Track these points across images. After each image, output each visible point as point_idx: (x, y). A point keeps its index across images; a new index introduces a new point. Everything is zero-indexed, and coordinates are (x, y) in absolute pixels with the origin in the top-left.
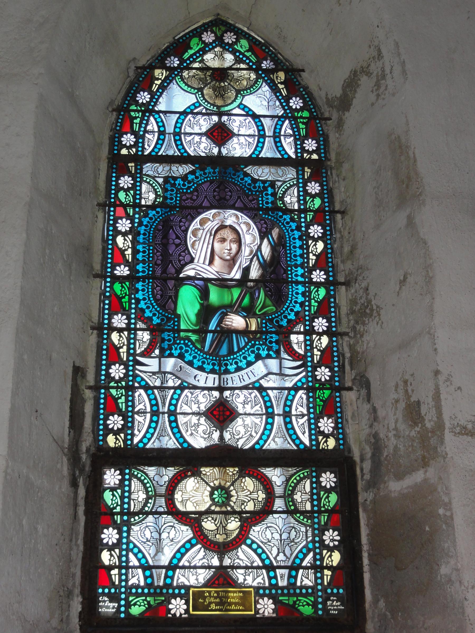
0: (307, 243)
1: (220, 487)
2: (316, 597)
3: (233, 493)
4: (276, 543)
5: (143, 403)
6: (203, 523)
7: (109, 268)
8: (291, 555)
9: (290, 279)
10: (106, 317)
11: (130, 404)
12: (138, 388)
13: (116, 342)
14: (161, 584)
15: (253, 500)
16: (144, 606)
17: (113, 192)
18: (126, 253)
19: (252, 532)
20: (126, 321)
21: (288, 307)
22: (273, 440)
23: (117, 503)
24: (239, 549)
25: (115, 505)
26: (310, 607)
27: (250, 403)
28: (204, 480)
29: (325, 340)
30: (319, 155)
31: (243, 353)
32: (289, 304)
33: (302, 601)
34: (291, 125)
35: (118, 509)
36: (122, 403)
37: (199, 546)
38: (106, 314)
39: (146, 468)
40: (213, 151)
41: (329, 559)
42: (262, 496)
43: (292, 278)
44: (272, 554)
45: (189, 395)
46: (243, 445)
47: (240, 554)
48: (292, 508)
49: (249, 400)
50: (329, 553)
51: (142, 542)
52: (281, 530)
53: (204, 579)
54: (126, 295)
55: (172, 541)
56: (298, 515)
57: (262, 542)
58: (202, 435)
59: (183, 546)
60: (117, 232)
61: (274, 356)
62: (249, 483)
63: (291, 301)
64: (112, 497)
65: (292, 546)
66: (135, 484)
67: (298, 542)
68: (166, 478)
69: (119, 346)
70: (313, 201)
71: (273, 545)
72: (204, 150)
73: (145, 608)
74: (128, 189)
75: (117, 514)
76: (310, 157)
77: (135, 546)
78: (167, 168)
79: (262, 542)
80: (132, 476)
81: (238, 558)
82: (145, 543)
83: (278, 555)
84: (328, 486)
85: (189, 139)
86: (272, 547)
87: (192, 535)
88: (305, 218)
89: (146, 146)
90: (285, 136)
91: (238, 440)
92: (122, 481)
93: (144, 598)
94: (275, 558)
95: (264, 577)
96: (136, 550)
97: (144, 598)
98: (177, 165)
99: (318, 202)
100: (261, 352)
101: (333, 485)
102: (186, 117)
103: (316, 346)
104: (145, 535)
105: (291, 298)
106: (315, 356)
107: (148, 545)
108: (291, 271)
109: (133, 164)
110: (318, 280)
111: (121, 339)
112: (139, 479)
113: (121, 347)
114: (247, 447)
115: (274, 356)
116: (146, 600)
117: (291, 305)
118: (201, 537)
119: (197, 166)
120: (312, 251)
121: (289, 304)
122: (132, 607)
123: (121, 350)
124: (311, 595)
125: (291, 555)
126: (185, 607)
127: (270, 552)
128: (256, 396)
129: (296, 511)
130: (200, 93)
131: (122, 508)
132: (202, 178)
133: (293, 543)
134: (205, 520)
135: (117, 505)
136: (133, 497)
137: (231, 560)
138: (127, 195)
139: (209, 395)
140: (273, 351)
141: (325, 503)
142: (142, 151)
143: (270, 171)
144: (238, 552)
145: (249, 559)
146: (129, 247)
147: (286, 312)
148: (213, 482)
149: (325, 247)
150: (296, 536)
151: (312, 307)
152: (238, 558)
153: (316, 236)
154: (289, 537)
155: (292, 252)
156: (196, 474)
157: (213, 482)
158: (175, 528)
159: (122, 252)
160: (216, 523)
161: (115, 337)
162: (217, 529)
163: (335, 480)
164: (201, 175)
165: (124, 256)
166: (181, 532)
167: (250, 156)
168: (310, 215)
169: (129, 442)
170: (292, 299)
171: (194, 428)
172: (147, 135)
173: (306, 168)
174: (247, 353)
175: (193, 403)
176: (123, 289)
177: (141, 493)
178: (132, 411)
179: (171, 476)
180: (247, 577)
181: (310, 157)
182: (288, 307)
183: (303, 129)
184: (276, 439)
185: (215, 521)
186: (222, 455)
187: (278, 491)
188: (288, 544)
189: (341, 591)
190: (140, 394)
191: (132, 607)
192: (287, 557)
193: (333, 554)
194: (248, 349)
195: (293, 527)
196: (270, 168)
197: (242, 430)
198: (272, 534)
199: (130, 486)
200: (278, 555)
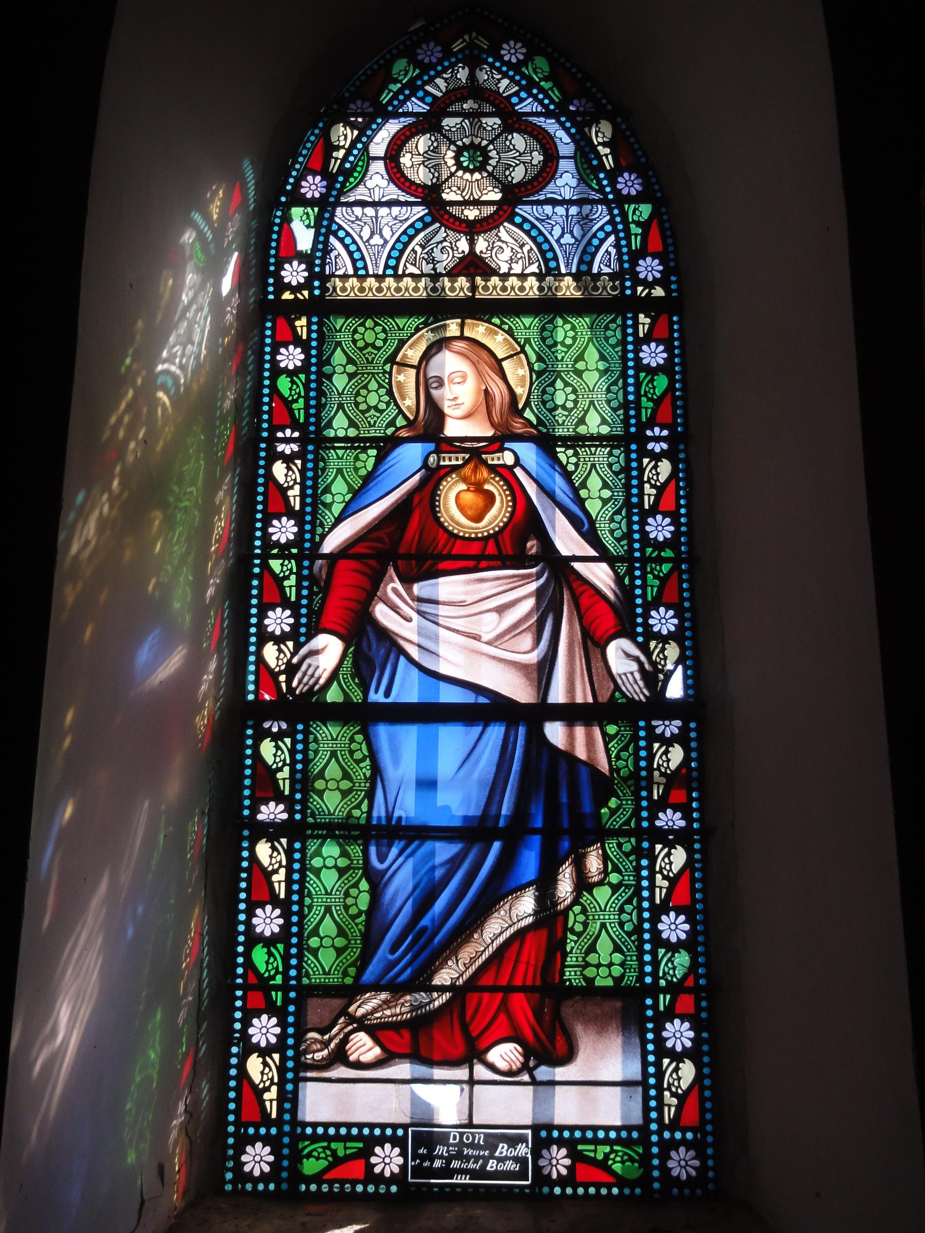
1: (472, 147)
2: (648, 1145)
3: (493, 154)
7: (263, 458)
8: (583, 236)
10: (268, 349)
13: (269, 760)
15: (524, 163)
16: (326, 1159)
17: (262, 463)
18: (290, 493)
20: (291, 621)
23: (272, 1079)
24: (501, 228)
25: (272, 973)
26: (636, 1165)
27: (520, 261)
30: (666, 288)
35: (279, 979)
36: (271, 1101)
41: (666, 860)
42: (538, 157)
44: (552, 236)
47: (503, 234)
50: (653, 463)
54: (285, 764)
55: (395, 219)
57: (537, 219)
59: (412, 226)
64: (262, 1066)
65: (585, 224)
69: (270, 868)
70: (652, 381)
73: (327, 1163)
75: (276, 988)
76: (649, 293)
77: (340, 228)
79: (537, 219)
81: (500, 240)
82: (353, 222)
83: (562, 236)
86: (553, 226)
94: (558, 241)
96: (341, 234)
99: (662, 382)
106: (657, 890)
111: (279, 753)
113: (276, 872)
116: (328, 1147)
124: (637, 1142)
125: (583, 236)
127: (550, 233)
128: (531, 249)
131: (286, 978)
135: (277, 972)
137: (489, 242)
138: (293, 382)
141: (651, 476)
144: (499, 231)
145: (516, 241)
148: (461, 140)
149: (686, 760)
152: (500, 240)
153: (650, 279)
154: (581, 212)
157: (461, 140)
159: (287, 404)
173: (641, 316)
176: (279, 753)
181: (649, 293)
183: (636, 235)
192: (576, 240)
193: (681, 1065)
200: (562, 236)
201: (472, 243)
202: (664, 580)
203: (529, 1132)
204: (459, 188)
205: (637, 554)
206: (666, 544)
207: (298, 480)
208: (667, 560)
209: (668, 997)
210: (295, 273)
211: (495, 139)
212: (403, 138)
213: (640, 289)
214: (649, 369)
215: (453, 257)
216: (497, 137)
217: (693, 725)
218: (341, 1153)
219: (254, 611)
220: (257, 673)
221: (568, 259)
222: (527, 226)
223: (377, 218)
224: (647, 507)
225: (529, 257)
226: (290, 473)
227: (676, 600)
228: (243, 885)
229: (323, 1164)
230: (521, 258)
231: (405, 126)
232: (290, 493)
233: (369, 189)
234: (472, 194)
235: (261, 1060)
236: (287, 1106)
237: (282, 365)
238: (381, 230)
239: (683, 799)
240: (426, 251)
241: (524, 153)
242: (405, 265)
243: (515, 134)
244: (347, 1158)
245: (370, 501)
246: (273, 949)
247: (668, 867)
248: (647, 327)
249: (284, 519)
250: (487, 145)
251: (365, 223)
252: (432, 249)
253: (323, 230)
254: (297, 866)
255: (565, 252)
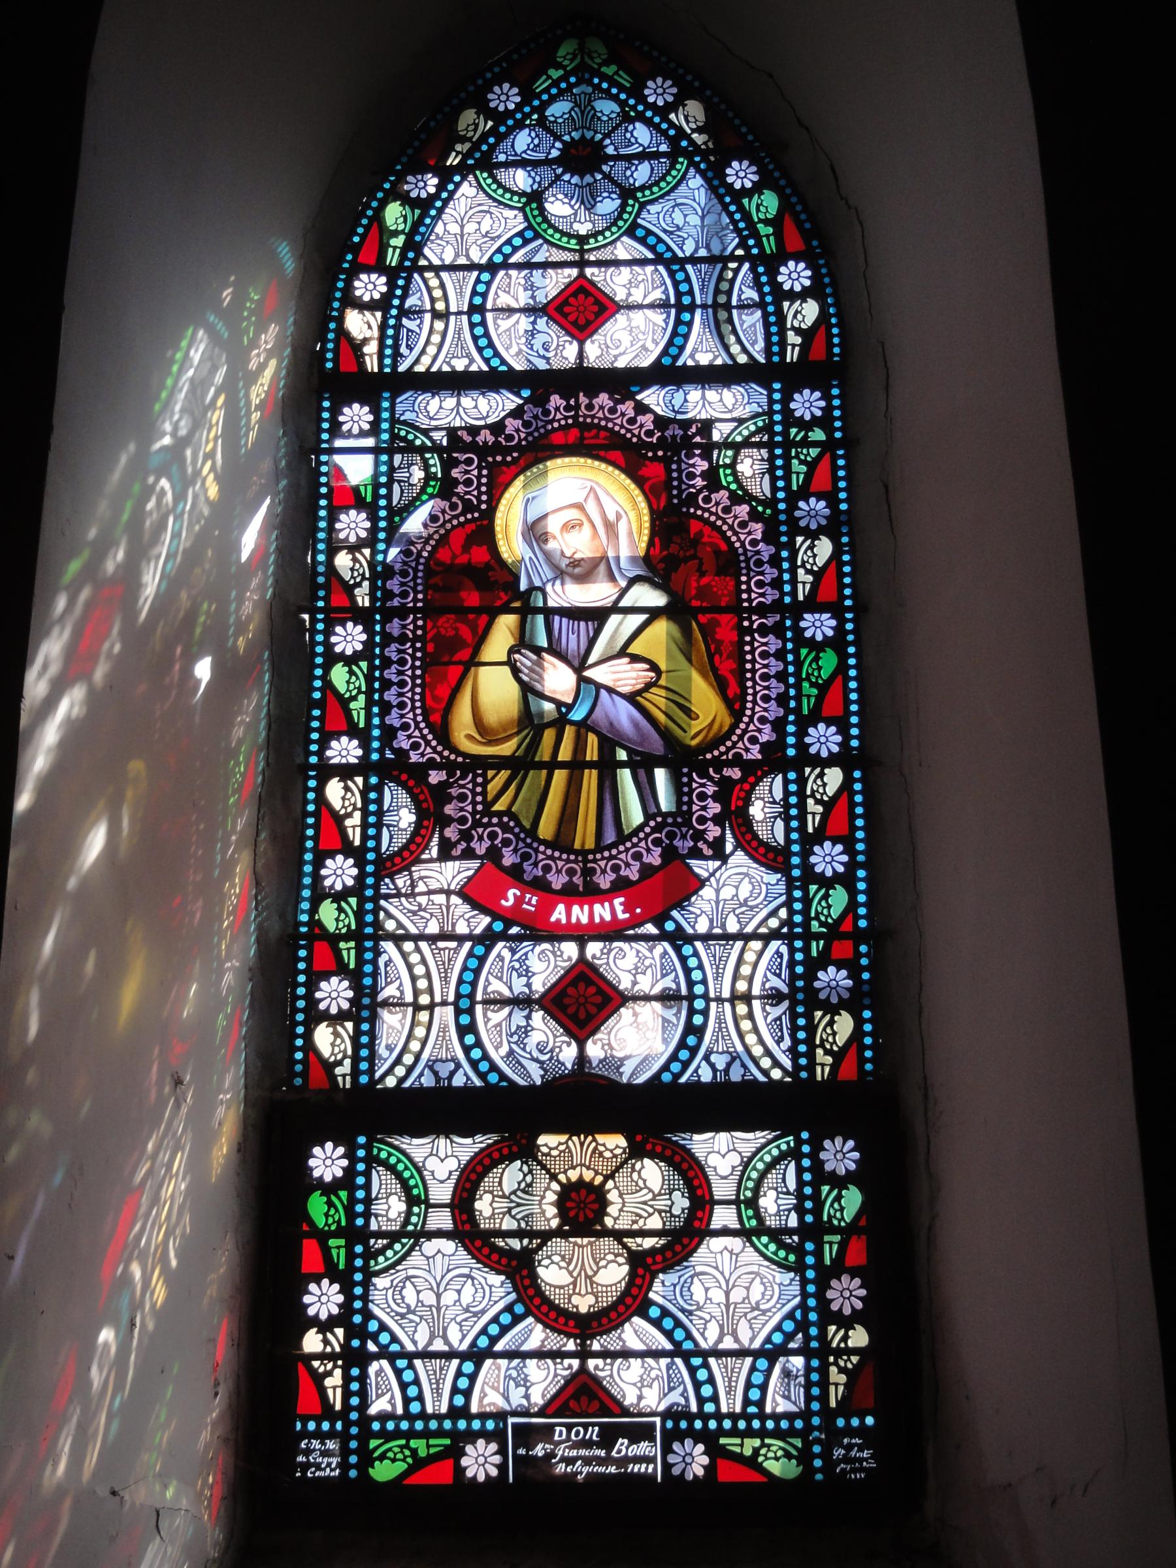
0: (792, 542)
4: (716, 1312)
5: (397, 984)
6: (540, 1270)
9: (746, 604)
11: (355, 1386)
12: (377, 1357)
14: (444, 1409)
16: (404, 1460)
18: (353, 705)
19: (657, 1286)
21: (745, 731)
22: (706, 1058)
27: (649, 971)
28: (544, 1167)
29: (834, 777)
30: (829, 431)
31: (635, 845)
32: (748, 724)
33: (774, 1448)
34: (757, 276)
36: (334, 1388)
37: (530, 1320)
38: (302, 959)
39: (407, 1140)
40: (565, 354)
42: (681, 1203)
43: (750, 600)
45: (507, 954)
46: (633, 1074)
48: (754, 1223)
49: (647, 962)
51: (398, 1314)
52: (727, 1282)
53: (543, 1396)
55: (467, 1310)
56: (765, 1239)
57: (665, 231)
58: (542, 352)
60: (315, 1016)
61: (708, 852)
62: (652, 1172)
63: (751, 718)
66: (380, 1180)
67: (769, 1310)
68: (452, 1164)
69: (343, 812)
71: (708, 1317)
72: (535, 1054)
74: (342, 1016)
77: (383, 1327)
78: (450, 402)
79: (665, 231)
80: (372, 1161)
84: (847, 1311)
85: (505, 324)
86: (707, 1321)
87: (513, 1296)
88: (818, 1253)
89: (403, 350)
90: (741, 307)
91: (616, 357)
92: (350, 1172)
93: (403, 1442)
95: (685, 1390)
97: (403, 1442)
98: (475, 394)
100: (677, 843)
101: (859, 1305)
102: (488, 950)
103: (813, 791)
104: (403, 1298)
105: (753, 709)
106: (810, 817)
107: (411, 1321)
108: (751, 643)
109: (342, 1242)
110: (817, 616)
111: (338, 1041)
112: (392, 1169)
113: (349, 815)
114: (641, 1080)
115: (710, 853)
116: (407, 1446)
117: (752, 727)
118: (532, 1300)
119: (526, 393)
120: (803, 562)
121: (748, 724)
122: (377, 1463)
123: (348, 822)
126: (497, 1459)
127: (702, 1335)
129: (761, 1230)
130: (534, 205)
132: (540, 424)
133: (756, 1313)
134: (546, 1262)
136: (387, 819)
139: (554, 953)
140: (706, 842)
142: (394, 365)
143: (703, 397)
146: (360, 692)
147: (740, 745)
148: (565, 1172)
150: (763, 1294)
151: (800, 586)
155: (757, 666)
156: (528, 1152)
158: (473, 1279)
160: (571, 1268)
161: (334, 790)
162: (574, 1284)
163: (863, 1292)
164: (536, 417)
165: (348, 712)
166: (487, 1289)
167: (658, 361)
168: (831, 1243)
169: (380, 557)
170: (754, 713)
171: (515, 1038)
172: (405, 321)
174: (643, 844)
175: (512, 1383)
177: (393, 1200)
178: (365, 1269)
179: (465, 1158)
180: (645, 1391)
182: (745, 731)
184: (713, 1058)
185: (569, 1264)
186: (584, 1100)
187: (722, 1189)
188: (745, 1314)
189: (870, 1420)
190: (390, 960)
191: (377, 1463)
193: (851, 1333)
194: (647, 835)
195: (757, 1274)
196: (703, 388)
197: (626, 339)
198: (707, 1290)
199: (367, 1187)
201: (581, 355)
202: (812, 466)
203: (658, 1420)
204: (563, 1258)
205: (778, 452)
206: (815, 422)
207: (359, 805)
208: (815, 444)
209: (822, 942)
210: (356, 418)
211: (610, 132)
212: (479, 1169)
213: (793, 431)
214: (812, 644)
215: (556, 1375)
216: (614, 182)
217: (857, 774)
218: (422, 1453)
219: (323, 513)
220: (336, 341)
221: (730, 1381)
222: (668, 1323)
223: (462, 236)
224: (810, 830)
225: (669, 1376)
226: (343, 916)
227: (845, 831)
228: (310, 832)
229: (401, 1467)
230: (657, 1377)
231: (482, 1150)
232: (353, 705)
233: (428, 1258)
234: (582, 1144)
235: (320, 1336)
236: (373, 795)
237: (338, 649)
238: (445, 1329)
239: (850, 955)
240: (516, 957)
241: (660, 1194)
242: (487, 980)
243: (646, 1160)
244: (431, 1459)
245: (454, 683)
246: (333, 1198)
247: (825, 912)
248: (808, 587)
249: (350, 625)
250: (603, 140)
251: (421, 1317)
252: (526, 954)
253: (354, 1416)
254: (373, 808)
255: (726, 1367)
